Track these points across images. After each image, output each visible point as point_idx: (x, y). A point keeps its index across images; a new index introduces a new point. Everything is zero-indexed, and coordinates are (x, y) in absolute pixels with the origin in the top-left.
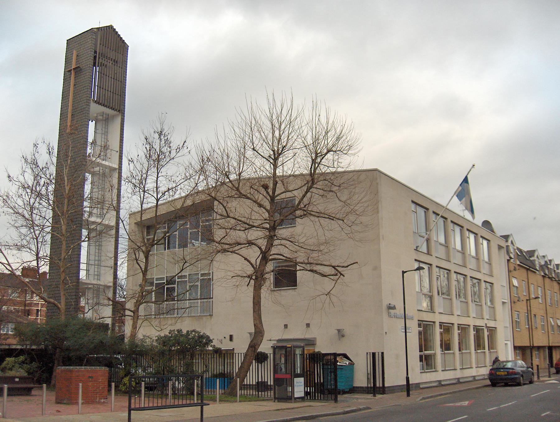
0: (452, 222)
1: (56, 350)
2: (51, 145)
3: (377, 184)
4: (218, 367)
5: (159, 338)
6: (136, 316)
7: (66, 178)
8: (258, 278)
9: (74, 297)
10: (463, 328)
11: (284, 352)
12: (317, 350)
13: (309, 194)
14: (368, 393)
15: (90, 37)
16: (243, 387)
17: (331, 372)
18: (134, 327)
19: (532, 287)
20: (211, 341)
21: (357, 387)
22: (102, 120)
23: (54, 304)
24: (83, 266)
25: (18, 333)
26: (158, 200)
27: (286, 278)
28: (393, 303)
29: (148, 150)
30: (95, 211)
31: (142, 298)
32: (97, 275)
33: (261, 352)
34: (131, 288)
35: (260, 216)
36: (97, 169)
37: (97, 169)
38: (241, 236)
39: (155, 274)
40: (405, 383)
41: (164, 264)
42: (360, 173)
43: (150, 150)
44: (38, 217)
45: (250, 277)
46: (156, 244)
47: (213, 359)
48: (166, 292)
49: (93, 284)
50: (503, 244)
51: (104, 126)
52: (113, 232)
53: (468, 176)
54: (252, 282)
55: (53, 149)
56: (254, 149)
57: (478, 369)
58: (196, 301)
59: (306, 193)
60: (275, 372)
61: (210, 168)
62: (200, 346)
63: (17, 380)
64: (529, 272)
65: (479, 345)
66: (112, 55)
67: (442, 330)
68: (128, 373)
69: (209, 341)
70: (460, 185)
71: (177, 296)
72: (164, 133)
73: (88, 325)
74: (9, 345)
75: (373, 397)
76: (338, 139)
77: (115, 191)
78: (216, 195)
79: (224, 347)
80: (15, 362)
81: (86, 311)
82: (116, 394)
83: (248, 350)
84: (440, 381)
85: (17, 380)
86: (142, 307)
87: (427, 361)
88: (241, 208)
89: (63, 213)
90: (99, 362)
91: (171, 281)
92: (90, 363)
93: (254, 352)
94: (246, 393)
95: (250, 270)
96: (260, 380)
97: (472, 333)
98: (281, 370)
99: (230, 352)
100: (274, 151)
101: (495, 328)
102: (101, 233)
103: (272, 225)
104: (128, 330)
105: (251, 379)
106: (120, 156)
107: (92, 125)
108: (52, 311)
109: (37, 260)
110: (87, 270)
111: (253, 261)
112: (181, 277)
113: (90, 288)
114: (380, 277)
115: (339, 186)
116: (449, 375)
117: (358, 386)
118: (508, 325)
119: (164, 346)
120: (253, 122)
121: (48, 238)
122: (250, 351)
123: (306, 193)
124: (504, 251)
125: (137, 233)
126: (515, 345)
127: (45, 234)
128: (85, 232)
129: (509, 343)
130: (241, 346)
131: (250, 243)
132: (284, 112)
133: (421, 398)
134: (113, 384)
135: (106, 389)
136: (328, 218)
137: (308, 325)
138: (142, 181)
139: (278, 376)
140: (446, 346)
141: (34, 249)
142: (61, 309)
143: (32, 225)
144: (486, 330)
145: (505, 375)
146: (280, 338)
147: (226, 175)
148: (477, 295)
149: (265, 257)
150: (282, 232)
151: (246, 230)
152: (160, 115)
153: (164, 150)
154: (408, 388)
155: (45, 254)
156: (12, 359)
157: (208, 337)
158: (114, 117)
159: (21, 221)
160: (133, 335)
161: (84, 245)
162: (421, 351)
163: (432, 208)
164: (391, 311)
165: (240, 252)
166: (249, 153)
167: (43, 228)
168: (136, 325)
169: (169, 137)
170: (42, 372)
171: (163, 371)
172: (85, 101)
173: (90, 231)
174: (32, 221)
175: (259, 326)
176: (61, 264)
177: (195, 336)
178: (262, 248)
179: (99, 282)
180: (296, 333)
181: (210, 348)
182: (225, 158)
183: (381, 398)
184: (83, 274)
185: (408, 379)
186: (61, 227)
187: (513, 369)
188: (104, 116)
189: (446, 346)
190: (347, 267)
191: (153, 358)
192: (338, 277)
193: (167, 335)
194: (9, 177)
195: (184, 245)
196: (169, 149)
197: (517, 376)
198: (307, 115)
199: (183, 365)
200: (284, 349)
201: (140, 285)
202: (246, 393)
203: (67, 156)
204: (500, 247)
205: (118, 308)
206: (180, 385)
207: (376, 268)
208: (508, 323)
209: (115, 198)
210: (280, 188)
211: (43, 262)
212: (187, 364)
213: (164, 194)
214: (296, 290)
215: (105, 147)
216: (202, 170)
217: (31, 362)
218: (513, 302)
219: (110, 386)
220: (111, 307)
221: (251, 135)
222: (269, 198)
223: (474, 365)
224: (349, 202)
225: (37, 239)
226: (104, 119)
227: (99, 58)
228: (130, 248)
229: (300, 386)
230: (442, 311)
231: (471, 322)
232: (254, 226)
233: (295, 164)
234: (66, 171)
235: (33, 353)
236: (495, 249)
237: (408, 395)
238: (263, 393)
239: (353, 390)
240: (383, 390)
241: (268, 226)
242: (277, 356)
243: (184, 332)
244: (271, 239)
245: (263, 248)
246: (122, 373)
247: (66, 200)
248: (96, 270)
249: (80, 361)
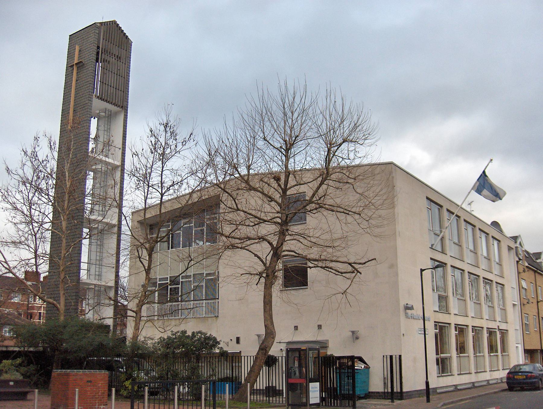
0: (465, 220)
1: (54, 352)
2: (53, 139)
3: (393, 177)
4: (223, 371)
5: (162, 340)
6: (139, 316)
7: (67, 174)
8: (268, 276)
9: (74, 297)
10: (477, 330)
11: (298, 355)
12: (329, 353)
13: (324, 187)
14: (384, 399)
15: (93, 31)
16: (254, 392)
17: (348, 377)
18: (137, 328)
20: (219, 343)
21: (372, 392)
22: (105, 117)
23: (53, 304)
24: (84, 266)
25: (18, 335)
26: (162, 195)
27: (297, 277)
28: (410, 303)
29: (153, 144)
30: (97, 207)
31: (145, 298)
32: (98, 275)
33: (273, 356)
34: (133, 287)
35: (271, 210)
36: (99, 167)
37: (99, 167)
38: (250, 232)
39: (160, 273)
41: (168, 264)
42: (374, 166)
43: (155, 144)
44: (37, 213)
45: (260, 274)
46: (159, 241)
47: (220, 363)
48: (170, 292)
49: (95, 285)
50: (513, 245)
51: (106, 122)
52: (116, 229)
53: (486, 171)
54: (263, 280)
55: (54, 144)
56: (265, 139)
57: (492, 372)
58: (202, 302)
59: (321, 185)
60: (289, 375)
61: (219, 160)
62: (206, 348)
63: (12, 383)
64: (536, 274)
65: (492, 348)
66: (115, 50)
67: (457, 332)
68: (129, 377)
69: (216, 343)
70: (478, 180)
71: (181, 296)
72: (169, 125)
73: (88, 326)
74: (7, 347)
75: (390, 403)
76: (356, 126)
77: (118, 186)
78: (224, 187)
79: (232, 349)
80: (12, 365)
81: (87, 312)
82: (116, 399)
83: (258, 354)
84: (456, 386)
85: (12, 383)
86: (144, 307)
87: (443, 365)
88: (252, 201)
89: (63, 210)
90: (100, 365)
91: (174, 281)
92: (90, 366)
93: (265, 354)
94: (255, 399)
95: (260, 268)
96: (270, 385)
97: (485, 335)
98: (295, 374)
99: (235, 355)
100: (285, 141)
101: (507, 330)
102: (101, 232)
103: (284, 219)
104: (129, 332)
105: (261, 383)
106: (122, 153)
107: (94, 122)
108: (51, 312)
109: (36, 258)
110: (88, 270)
111: (263, 258)
112: (187, 277)
113: (91, 288)
114: (397, 275)
115: (355, 179)
116: (465, 380)
117: (374, 391)
118: (518, 328)
119: (168, 348)
120: (264, 111)
121: (48, 235)
122: (260, 353)
123: (321, 185)
124: (513, 252)
125: (140, 229)
126: (527, 348)
127: (44, 231)
128: (86, 230)
129: (519, 346)
130: (249, 349)
131: (262, 239)
132: (297, 100)
133: (442, 404)
134: (114, 389)
135: (106, 393)
136: (343, 212)
137: (320, 327)
138: (146, 178)
139: (291, 381)
140: (461, 349)
141: (33, 246)
142: (60, 310)
143: (30, 221)
144: (498, 333)
145: (524, 379)
146: (290, 340)
147: (235, 167)
148: (489, 298)
149: (276, 253)
150: (295, 228)
151: (255, 225)
152: (166, 105)
153: (170, 142)
154: (428, 392)
155: (44, 252)
156: (10, 361)
157: (215, 339)
158: (116, 114)
159: (19, 218)
160: (135, 337)
161: (86, 242)
162: (437, 354)
163: (446, 206)
164: (408, 311)
165: (251, 248)
166: (260, 143)
167: (42, 224)
168: (139, 327)
169: (175, 129)
170: (40, 375)
171: (167, 374)
172: (88, 96)
173: (91, 229)
174: (31, 217)
175: (271, 327)
176: (61, 262)
177: (201, 337)
178: (273, 243)
179: (98, 283)
180: (307, 335)
181: (217, 351)
182: (234, 149)
183: (400, 404)
184: (83, 275)
185: (427, 383)
186: (61, 222)
187: (531, 373)
188: (107, 112)
189: (461, 349)
190: (364, 263)
191: (156, 362)
192: (354, 274)
193: (170, 337)
194: (8, 170)
195: (188, 243)
196: (174, 142)
197: (536, 380)
198: (322, 103)
200: (296, 353)
201: (143, 286)
202: (255, 399)
203: (69, 149)
204: (510, 248)
205: (120, 312)
206: (185, 389)
207: (393, 266)
208: (518, 326)
209: (118, 195)
210: (292, 181)
211: (42, 261)
212: (192, 368)
213: (168, 189)
214: (306, 290)
215: (108, 144)
216: (211, 163)
217: (28, 365)
218: (522, 305)
219: (110, 390)
220: (112, 307)
221: (262, 124)
222: (280, 191)
223: (488, 369)
224: (366, 194)
225: (35, 236)
226: (107, 115)
227: (102, 53)
228: (133, 245)
229: (315, 391)
230: (457, 313)
231: (485, 324)
232: (265, 221)
233: (308, 157)
234: (67, 166)
235: (31, 355)
236: (505, 250)
237: (428, 400)
238: (274, 399)
239: (369, 395)
240: (401, 395)
241: (279, 220)
242: (291, 361)
243: (189, 333)
244: (282, 233)
245: (275, 243)
246: (123, 377)
247: (67, 196)
248: (97, 270)
249: (79, 364)
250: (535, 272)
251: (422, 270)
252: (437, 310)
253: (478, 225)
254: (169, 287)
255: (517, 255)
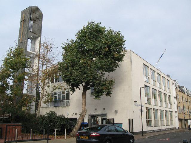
19: (183, 99)
36: (31, 55)
40: (141, 131)
87: (149, 123)
116: (157, 128)
137: (104, 109)
158: (38, 37)
162: (147, 119)
179: (31, 95)
184: (25, 92)
185: (142, 129)
199: (65, 126)
250: (182, 92)
251: (141, 88)
252: (147, 103)
253: (162, 75)
254: (54, 96)
255: (176, 86)
